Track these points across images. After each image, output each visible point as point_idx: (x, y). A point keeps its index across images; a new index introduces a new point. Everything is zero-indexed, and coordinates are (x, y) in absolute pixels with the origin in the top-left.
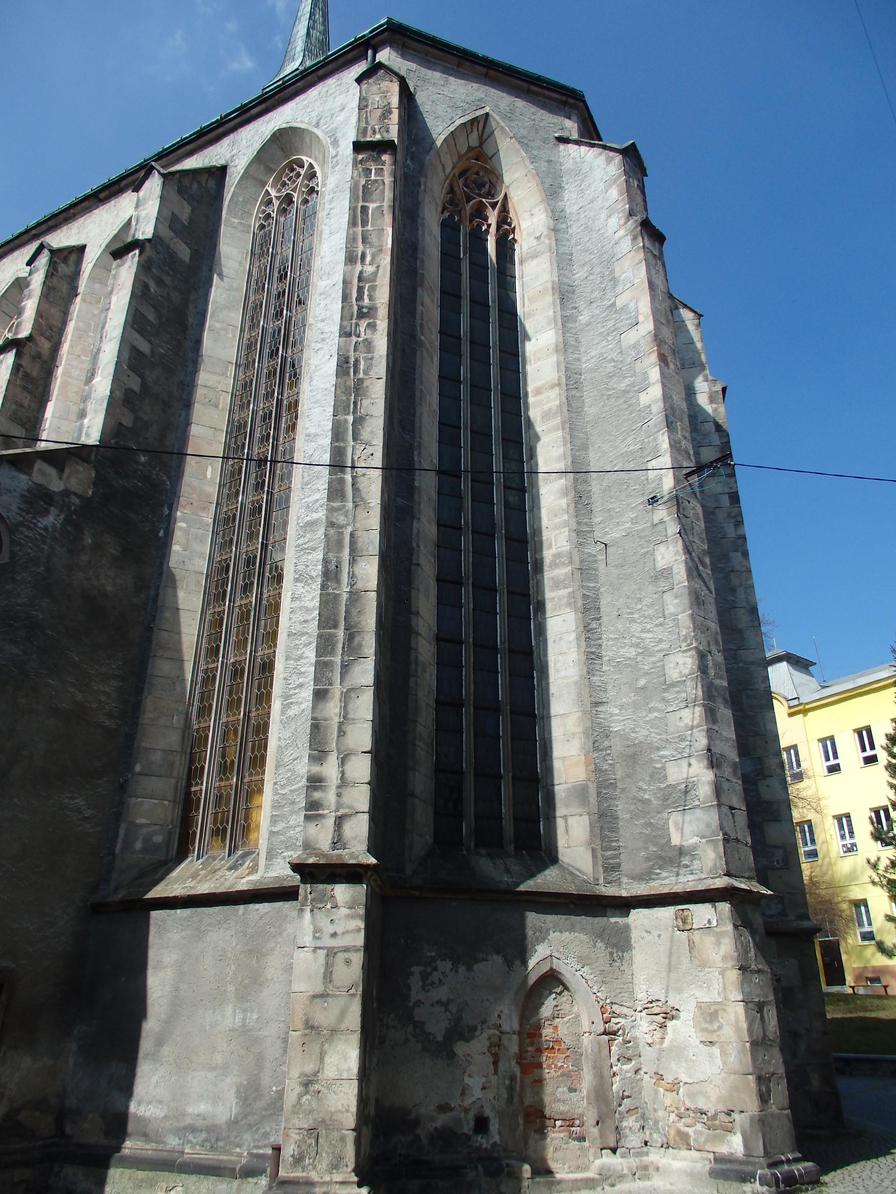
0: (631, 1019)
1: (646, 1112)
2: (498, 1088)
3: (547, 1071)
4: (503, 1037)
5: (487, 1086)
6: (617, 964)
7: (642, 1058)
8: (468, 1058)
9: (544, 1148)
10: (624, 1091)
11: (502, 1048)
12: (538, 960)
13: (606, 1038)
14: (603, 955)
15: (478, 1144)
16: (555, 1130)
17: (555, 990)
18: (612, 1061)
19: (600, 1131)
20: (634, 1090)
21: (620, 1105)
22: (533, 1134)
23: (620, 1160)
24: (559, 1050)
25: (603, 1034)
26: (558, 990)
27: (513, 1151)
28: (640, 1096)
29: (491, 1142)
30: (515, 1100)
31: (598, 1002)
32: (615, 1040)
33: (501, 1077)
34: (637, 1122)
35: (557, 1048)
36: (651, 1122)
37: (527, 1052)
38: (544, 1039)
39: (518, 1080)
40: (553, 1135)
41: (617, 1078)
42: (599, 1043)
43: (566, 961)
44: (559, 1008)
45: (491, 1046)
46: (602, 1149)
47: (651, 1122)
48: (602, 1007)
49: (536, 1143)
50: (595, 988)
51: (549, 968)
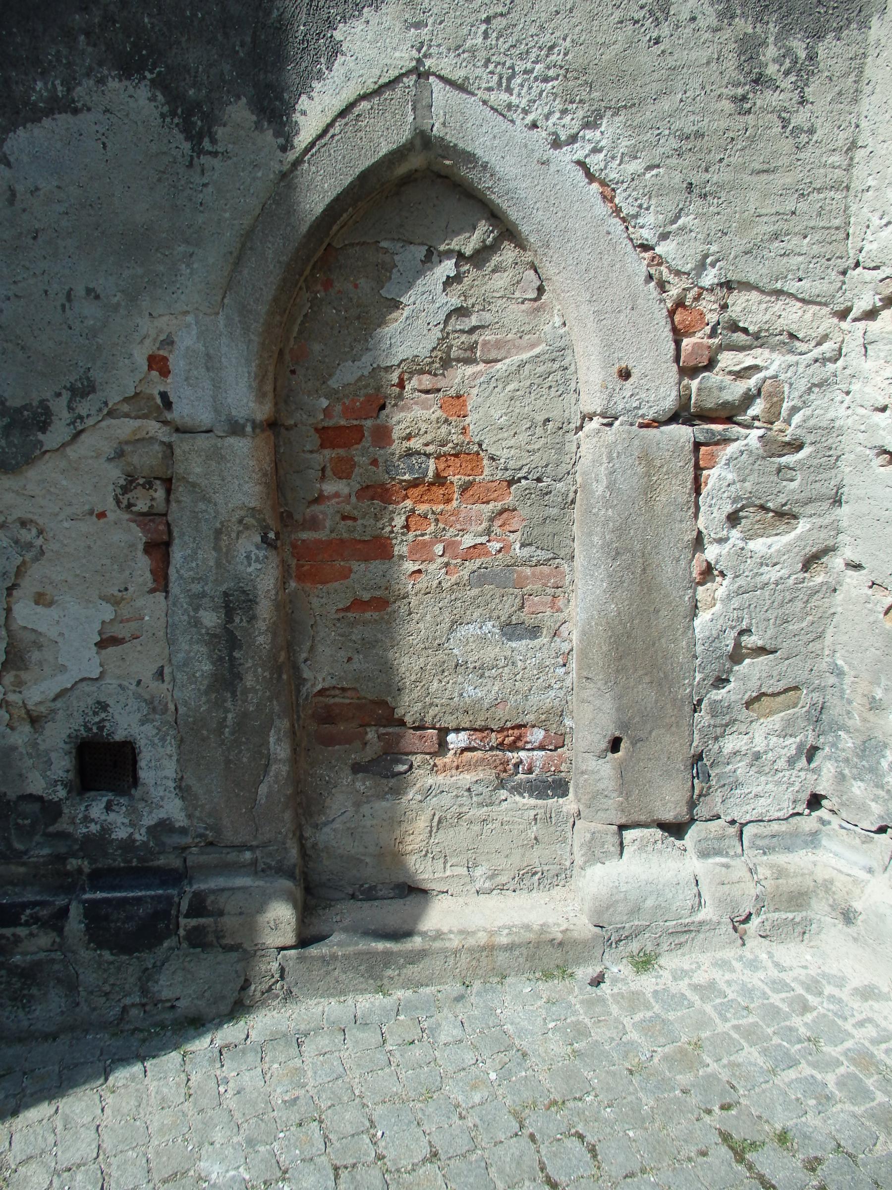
0: (817, 352)
1: (833, 701)
2: (171, 642)
3: (410, 566)
4: (183, 446)
5: (119, 631)
6: (772, 98)
7: (845, 510)
8: (26, 535)
9: (395, 821)
10: (747, 631)
11: (180, 491)
12: (349, 94)
13: (683, 433)
14: (702, 55)
15: (94, 828)
16: (439, 761)
17: (455, 244)
18: (701, 524)
19: (622, 772)
20: (792, 627)
21: (721, 682)
22: (346, 778)
23: (694, 865)
24: (465, 488)
25: (674, 418)
26: (469, 243)
27: (243, 847)
28: (815, 646)
29: (148, 821)
30: (249, 681)
31: (662, 286)
32: (726, 441)
33: (183, 600)
34: (784, 734)
35: (457, 479)
36: (847, 742)
37: (319, 499)
38: (398, 447)
39: (265, 609)
40: (430, 781)
41: (721, 588)
42: (646, 457)
43: (500, 98)
44: (474, 320)
45: (130, 484)
46: (622, 828)
47: (847, 742)
48: (680, 304)
49: (357, 805)
50: (649, 219)
51: (404, 135)
